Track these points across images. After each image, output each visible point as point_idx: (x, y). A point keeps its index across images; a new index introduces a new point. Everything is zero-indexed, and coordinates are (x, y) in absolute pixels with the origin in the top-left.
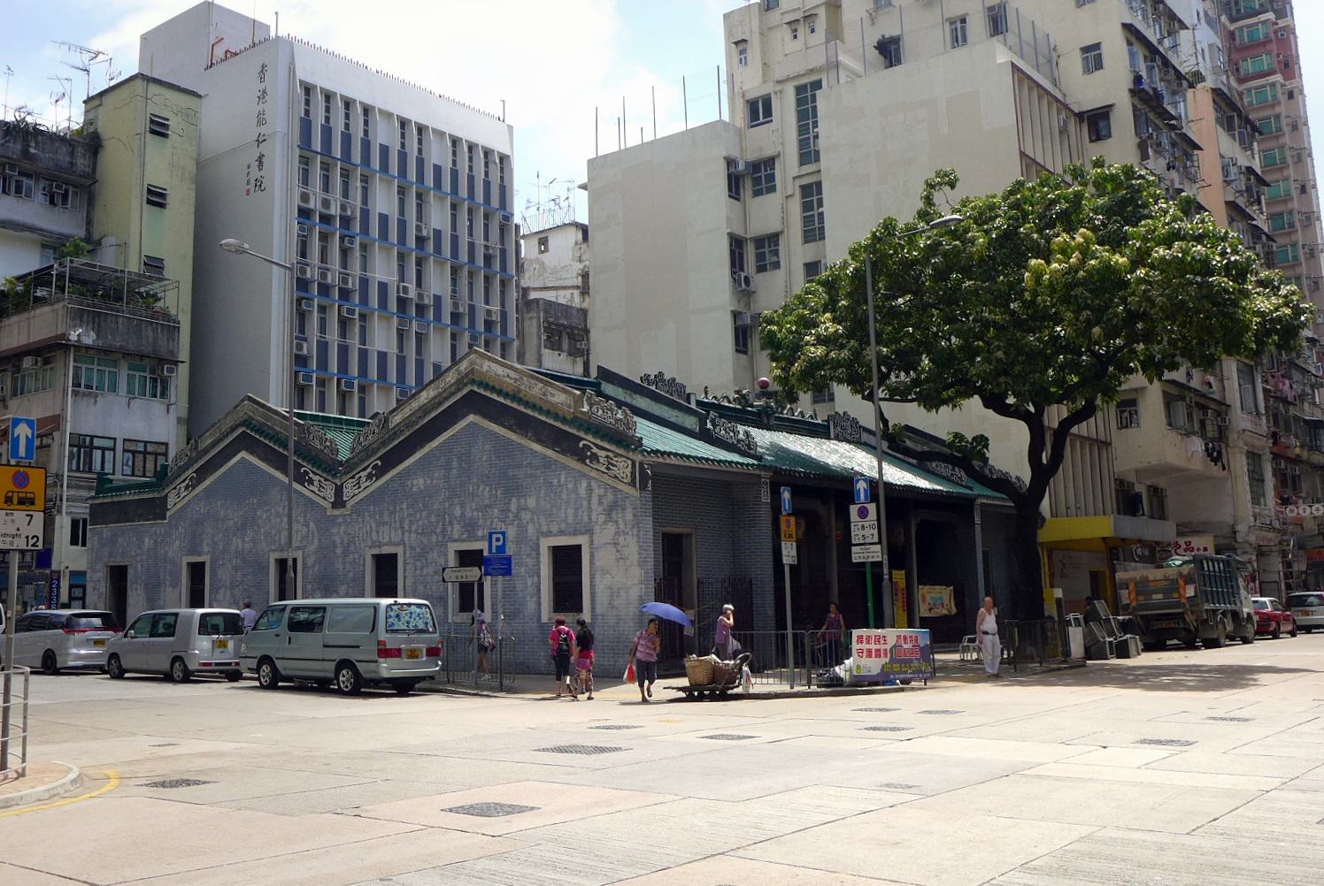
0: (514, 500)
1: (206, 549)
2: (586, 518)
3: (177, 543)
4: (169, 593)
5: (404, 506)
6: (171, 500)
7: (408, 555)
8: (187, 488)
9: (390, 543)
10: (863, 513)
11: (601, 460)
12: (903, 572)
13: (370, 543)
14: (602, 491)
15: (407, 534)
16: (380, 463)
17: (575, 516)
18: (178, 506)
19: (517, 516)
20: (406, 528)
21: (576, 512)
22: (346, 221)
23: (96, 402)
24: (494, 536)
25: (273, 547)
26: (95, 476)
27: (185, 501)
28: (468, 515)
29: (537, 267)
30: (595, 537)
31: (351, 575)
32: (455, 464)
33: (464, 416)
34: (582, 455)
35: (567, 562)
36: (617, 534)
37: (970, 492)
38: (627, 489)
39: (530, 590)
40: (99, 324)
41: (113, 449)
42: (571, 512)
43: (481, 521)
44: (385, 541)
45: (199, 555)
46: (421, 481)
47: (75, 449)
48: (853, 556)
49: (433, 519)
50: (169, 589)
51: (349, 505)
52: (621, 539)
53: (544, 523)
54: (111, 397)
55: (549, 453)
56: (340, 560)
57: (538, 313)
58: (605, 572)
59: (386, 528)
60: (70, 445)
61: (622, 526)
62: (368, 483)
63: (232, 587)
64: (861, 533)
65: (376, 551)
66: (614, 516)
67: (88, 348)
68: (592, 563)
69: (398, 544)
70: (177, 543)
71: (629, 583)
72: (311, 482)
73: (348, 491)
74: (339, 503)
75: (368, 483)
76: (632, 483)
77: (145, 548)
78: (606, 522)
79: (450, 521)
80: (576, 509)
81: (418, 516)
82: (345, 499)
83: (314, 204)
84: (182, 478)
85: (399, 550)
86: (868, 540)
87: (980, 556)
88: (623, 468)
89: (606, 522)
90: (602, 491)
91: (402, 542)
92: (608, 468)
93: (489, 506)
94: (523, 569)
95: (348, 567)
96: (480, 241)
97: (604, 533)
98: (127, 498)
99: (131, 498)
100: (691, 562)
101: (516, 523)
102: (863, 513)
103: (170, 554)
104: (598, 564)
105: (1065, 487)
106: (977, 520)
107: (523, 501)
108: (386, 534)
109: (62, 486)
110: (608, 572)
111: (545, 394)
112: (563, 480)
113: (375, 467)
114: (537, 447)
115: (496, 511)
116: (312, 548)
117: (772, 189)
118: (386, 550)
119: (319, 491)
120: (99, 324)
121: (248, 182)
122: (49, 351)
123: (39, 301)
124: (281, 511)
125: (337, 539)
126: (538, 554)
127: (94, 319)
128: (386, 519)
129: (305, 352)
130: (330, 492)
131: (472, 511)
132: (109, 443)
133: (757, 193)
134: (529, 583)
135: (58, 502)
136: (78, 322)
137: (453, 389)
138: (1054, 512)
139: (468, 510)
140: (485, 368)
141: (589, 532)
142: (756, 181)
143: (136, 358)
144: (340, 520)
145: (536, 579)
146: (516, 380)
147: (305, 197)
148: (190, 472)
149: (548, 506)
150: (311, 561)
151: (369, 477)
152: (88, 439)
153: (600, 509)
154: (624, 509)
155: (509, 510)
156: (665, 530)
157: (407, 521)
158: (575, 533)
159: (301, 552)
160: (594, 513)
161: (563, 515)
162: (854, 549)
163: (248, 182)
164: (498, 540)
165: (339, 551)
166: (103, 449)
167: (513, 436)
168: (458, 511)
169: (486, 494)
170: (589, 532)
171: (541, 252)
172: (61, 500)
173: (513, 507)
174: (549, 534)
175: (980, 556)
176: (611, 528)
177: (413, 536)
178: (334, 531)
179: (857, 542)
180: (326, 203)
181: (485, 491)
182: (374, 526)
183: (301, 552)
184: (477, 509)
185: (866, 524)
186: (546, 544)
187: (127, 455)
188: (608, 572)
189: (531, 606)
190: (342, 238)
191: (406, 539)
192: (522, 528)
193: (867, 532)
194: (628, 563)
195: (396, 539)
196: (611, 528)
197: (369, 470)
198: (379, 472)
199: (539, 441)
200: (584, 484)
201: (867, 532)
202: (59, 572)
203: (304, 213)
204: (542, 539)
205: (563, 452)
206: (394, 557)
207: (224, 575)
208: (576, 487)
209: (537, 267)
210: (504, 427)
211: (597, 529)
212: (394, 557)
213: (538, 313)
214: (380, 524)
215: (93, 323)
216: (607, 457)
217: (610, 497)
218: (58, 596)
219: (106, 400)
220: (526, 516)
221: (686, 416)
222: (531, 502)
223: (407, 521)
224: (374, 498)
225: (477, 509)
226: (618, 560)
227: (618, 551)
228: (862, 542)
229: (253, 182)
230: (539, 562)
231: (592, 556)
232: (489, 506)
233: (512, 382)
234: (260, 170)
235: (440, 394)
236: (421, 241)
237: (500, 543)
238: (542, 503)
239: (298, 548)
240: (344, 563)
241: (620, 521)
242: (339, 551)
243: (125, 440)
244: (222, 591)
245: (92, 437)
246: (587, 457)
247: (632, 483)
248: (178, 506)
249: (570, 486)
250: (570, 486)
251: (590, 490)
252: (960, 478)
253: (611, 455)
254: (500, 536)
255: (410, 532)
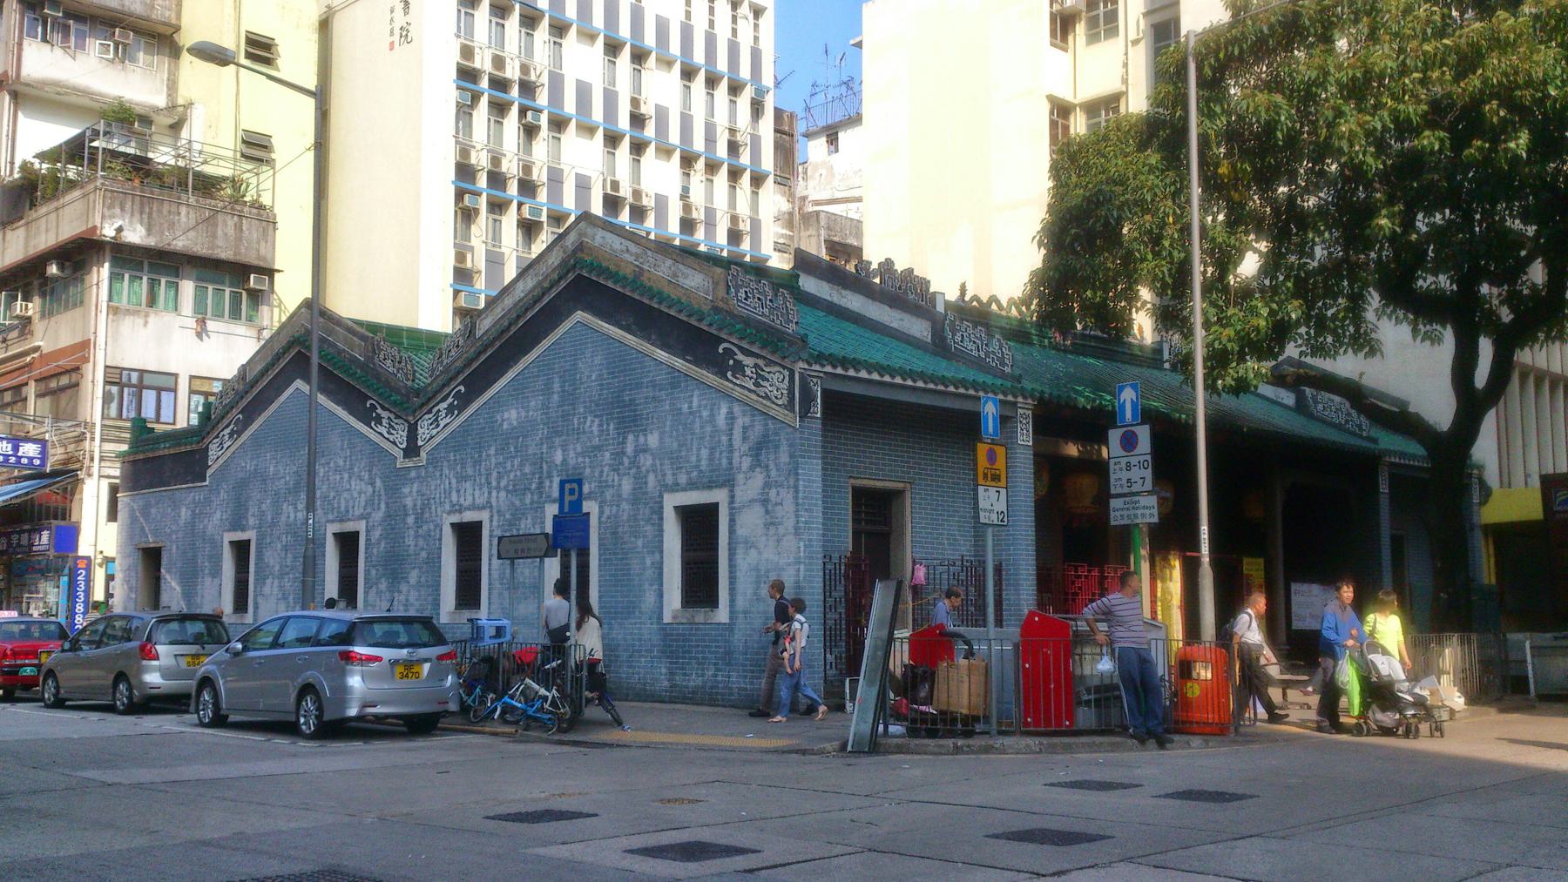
0: (631, 437)
1: (252, 521)
2: (724, 461)
3: (218, 515)
4: (207, 587)
5: (492, 451)
6: (213, 452)
7: (495, 523)
8: (231, 435)
9: (473, 507)
10: (1129, 442)
11: (748, 372)
12: (1261, 561)
13: (447, 507)
14: (747, 420)
15: (494, 494)
16: (462, 388)
17: (711, 459)
18: (221, 461)
19: (634, 463)
20: (494, 484)
21: (711, 454)
22: (528, 88)
23: (146, 323)
24: (568, 486)
25: (330, 517)
26: (128, 424)
27: (229, 453)
28: (572, 462)
29: (824, 172)
30: (738, 492)
31: (424, 554)
32: (556, 386)
33: (570, 313)
34: (721, 365)
35: (700, 525)
36: (767, 485)
37: (1372, 446)
38: (781, 414)
39: (649, 573)
40: (150, 214)
41: (175, 390)
42: (705, 453)
43: (588, 471)
44: (466, 504)
45: (243, 530)
46: (513, 414)
47: (115, 389)
48: (1112, 514)
49: (527, 470)
50: (208, 580)
51: (423, 454)
52: (773, 492)
53: (669, 472)
54: (169, 318)
55: (679, 363)
56: (412, 532)
57: (818, 230)
58: (750, 545)
59: (468, 485)
60: (106, 383)
61: (773, 473)
62: (448, 420)
63: (282, 575)
64: (1125, 475)
65: (455, 519)
66: (763, 458)
67: (133, 248)
68: (732, 531)
69: (483, 508)
70: (218, 515)
71: (782, 561)
72: (379, 420)
73: (424, 431)
74: (412, 450)
75: (448, 420)
76: (790, 406)
77: (182, 522)
78: (752, 468)
79: (549, 472)
80: (712, 449)
81: (509, 465)
82: (420, 443)
83: (482, 62)
84: (226, 421)
85: (484, 516)
86: (1135, 488)
87: (1386, 541)
88: (777, 383)
89: (752, 468)
90: (747, 420)
91: (488, 505)
92: (757, 384)
93: (599, 448)
94: (640, 543)
95: (421, 542)
96: (721, 119)
97: (750, 486)
98: (161, 453)
99: (167, 452)
100: (903, 534)
101: (633, 471)
102: (1129, 442)
103: (210, 530)
104: (741, 532)
105: (1524, 446)
106: (1384, 488)
107: (642, 439)
108: (471, 493)
109: (93, 439)
110: (753, 546)
111: (675, 275)
112: (695, 404)
113: (458, 395)
114: (661, 355)
115: (607, 454)
116: (378, 516)
117: (1112, 31)
118: (469, 516)
119: (388, 436)
120: (150, 214)
121: (392, 33)
122: (79, 253)
123: (72, 185)
124: (341, 463)
125: (409, 502)
126: (661, 519)
127: (142, 204)
128: (470, 471)
129: (469, 264)
130: (401, 435)
131: (578, 455)
132: (169, 382)
133: (1093, 38)
134: (648, 562)
135: (87, 462)
136: (118, 211)
137: (555, 276)
138: (1506, 480)
139: (572, 454)
140: (598, 241)
141: (728, 482)
142: (1093, 23)
143: (209, 268)
144: (413, 474)
145: (657, 556)
146: (637, 257)
147: (467, 52)
148: (235, 414)
149: (675, 445)
150: (377, 534)
151: (450, 410)
152: (135, 376)
153: (745, 448)
154: (777, 447)
155: (624, 453)
156: (859, 483)
157: (495, 474)
158: (710, 486)
159: (363, 523)
160: (736, 454)
161: (694, 459)
162: (1114, 503)
163: (392, 33)
164: (572, 492)
165: (410, 520)
166: (159, 390)
167: (630, 339)
168: (558, 457)
169: (595, 428)
170: (728, 482)
171: (830, 153)
172: (92, 459)
173: (630, 449)
174: (675, 488)
175: (1386, 541)
176: (758, 479)
177: (503, 494)
178: (406, 490)
179: (1119, 491)
180: (499, 62)
181: (593, 425)
182: (454, 481)
183: (363, 523)
184: (582, 454)
185: (1134, 461)
186: (671, 501)
187: (195, 398)
188: (753, 546)
189: (650, 598)
190: (523, 112)
191: (493, 500)
192: (640, 481)
193: (1136, 474)
194: (781, 530)
195: (479, 501)
196: (758, 479)
197: (450, 400)
198: (464, 401)
199: (664, 346)
200: (724, 410)
201: (1136, 474)
202: (88, 558)
203: (467, 75)
204: (666, 496)
205: (696, 363)
206: (478, 525)
207: (272, 558)
208: (712, 415)
209: (824, 172)
210: (621, 327)
211: (740, 478)
212: (478, 525)
213: (818, 230)
214: (462, 478)
215: (141, 213)
216: (756, 366)
217: (758, 428)
218: (88, 591)
219: (160, 320)
220: (646, 461)
221: (914, 319)
222: (653, 440)
223: (495, 474)
224: (456, 442)
225: (582, 454)
226: (767, 526)
227: (767, 512)
228: (1126, 490)
229: (397, 32)
230: (661, 531)
231: (732, 521)
232: (599, 448)
233: (632, 259)
234: (406, 13)
235: (540, 283)
236: (637, 120)
237: (574, 498)
238: (668, 440)
239: (361, 517)
240: (417, 536)
241: (772, 466)
242: (410, 520)
243: (192, 377)
244: (269, 581)
245: (142, 372)
246: (728, 368)
247: (790, 406)
248: (221, 461)
249: (705, 414)
250: (705, 414)
251: (731, 417)
252: (1360, 426)
253: (761, 362)
254: (575, 486)
255: (498, 488)
